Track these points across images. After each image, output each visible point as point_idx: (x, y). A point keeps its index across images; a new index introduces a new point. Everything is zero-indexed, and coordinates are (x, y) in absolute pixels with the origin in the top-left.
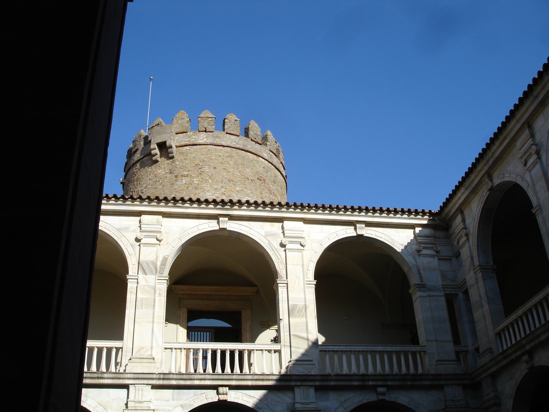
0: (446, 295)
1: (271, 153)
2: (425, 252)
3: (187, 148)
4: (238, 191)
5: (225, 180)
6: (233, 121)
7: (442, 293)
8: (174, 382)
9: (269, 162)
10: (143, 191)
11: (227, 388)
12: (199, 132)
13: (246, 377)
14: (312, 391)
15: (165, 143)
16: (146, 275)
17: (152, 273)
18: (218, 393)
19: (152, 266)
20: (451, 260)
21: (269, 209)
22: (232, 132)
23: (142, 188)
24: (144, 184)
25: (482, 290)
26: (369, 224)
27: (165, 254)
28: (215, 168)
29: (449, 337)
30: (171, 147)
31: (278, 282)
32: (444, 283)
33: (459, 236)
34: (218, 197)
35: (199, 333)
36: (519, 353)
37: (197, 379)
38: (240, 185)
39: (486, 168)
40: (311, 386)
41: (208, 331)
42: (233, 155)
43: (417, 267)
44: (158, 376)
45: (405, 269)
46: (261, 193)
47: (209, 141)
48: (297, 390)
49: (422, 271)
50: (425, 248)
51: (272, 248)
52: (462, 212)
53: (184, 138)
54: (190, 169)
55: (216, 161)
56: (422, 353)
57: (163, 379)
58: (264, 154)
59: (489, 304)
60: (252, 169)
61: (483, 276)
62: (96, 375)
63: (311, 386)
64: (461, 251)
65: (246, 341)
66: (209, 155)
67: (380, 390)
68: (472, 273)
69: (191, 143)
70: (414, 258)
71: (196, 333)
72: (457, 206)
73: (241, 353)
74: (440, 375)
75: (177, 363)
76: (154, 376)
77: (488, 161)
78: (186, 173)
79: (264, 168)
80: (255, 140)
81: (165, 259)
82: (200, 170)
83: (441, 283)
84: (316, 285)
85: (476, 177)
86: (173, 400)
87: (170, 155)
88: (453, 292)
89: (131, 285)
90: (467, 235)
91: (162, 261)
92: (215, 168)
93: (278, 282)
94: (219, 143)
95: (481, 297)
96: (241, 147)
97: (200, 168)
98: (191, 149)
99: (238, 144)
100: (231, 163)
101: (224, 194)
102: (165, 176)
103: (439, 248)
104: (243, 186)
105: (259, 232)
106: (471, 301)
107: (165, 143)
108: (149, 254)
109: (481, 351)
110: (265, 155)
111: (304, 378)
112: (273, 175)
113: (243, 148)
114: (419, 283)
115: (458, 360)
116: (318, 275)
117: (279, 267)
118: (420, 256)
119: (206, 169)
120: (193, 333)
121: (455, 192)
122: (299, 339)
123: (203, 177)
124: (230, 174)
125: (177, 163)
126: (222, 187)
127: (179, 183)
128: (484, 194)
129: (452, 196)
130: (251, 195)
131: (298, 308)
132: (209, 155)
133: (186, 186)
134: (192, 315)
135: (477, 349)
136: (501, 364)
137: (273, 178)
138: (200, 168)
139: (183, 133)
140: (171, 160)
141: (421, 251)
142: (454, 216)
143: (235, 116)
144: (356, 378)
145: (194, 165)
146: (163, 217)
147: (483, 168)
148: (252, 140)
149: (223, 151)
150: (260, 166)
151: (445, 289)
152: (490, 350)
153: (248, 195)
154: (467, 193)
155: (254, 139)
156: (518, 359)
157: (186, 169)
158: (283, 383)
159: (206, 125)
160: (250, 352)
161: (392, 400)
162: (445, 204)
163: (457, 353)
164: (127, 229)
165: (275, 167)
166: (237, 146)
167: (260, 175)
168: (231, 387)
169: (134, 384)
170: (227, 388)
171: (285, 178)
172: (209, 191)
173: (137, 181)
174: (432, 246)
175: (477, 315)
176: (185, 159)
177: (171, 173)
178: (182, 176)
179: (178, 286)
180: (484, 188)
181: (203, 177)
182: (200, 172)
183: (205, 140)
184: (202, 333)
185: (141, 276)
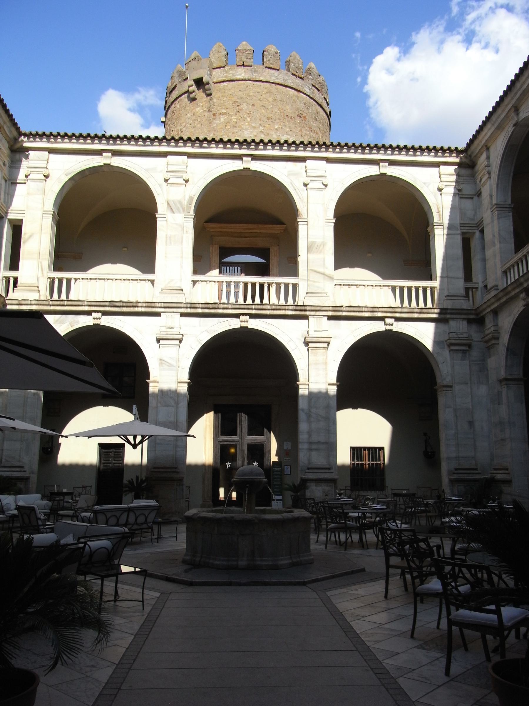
0: (463, 233)
1: (313, 88)
3: (225, 84)
4: (276, 129)
5: (263, 118)
6: (273, 54)
7: (459, 232)
8: (200, 311)
9: (311, 98)
10: (182, 130)
11: (394, 319)
12: (237, 66)
13: (264, 307)
14: (465, 323)
16: (174, 213)
17: (180, 212)
18: (386, 325)
19: (178, 205)
20: (472, 198)
21: (295, 149)
23: (181, 128)
24: (183, 123)
25: (496, 229)
26: (392, 163)
29: (461, 274)
30: (208, 83)
31: (298, 220)
32: (462, 222)
33: (482, 174)
34: (256, 136)
35: (228, 268)
36: (517, 290)
37: (220, 308)
38: (279, 122)
39: (513, 101)
40: (464, 319)
41: (239, 266)
42: (273, 91)
44: (185, 306)
46: (301, 131)
47: (247, 77)
51: (294, 188)
52: (488, 149)
54: (229, 106)
55: (254, 98)
56: (474, 290)
57: (190, 308)
59: (500, 242)
60: (292, 105)
61: (498, 215)
62: (226, 306)
63: (464, 319)
64: (482, 190)
65: (274, 275)
68: (489, 211)
69: (229, 79)
71: (231, 268)
72: (483, 142)
73: (262, 286)
76: (182, 305)
77: (516, 93)
78: (224, 111)
79: (305, 104)
81: (191, 198)
82: (237, 108)
83: (458, 222)
84: (335, 223)
85: (503, 111)
87: (208, 92)
89: (160, 224)
90: (489, 173)
92: (253, 105)
93: (298, 220)
94: (257, 78)
95: (494, 236)
96: (281, 82)
97: (238, 106)
98: (229, 85)
99: (277, 79)
100: (270, 99)
101: (263, 132)
102: (203, 115)
104: (282, 124)
105: (284, 173)
106: (485, 240)
109: (488, 288)
110: (307, 91)
112: (315, 111)
113: (283, 84)
115: (467, 296)
116: (337, 215)
117: (300, 205)
119: (244, 106)
120: (233, 268)
121: (481, 128)
122: (315, 273)
124: (268, 111)
125: (215, 100)
126: (260, 125)
127: (217, 121)
128: (510, 129)
129: (478, 132)
130: (290, 133)
131: (316, 245)
133: (224, 124)
134: (225, 252)
135: (486, 286)
136: (502, 301)
137: (314, 115)
138: (238, 106)
139: (220, 68)
140: (209, 98)
142: (480, 153)
143: (275, 47)
144: (367, 309)
145: (231, 102)
146: (188, 157)
147: (510, 102)
148: (293, 74)
149: (262, 87)
150: (301, 102)
151: (462, 228)
152: (495, 287)
153: (287, 133)
154: (493, 129)
155: (295, 73)
156: (517, 296)
157: (224, 107)
158: (443, 316)
159: (244, 59)
160: (269, 285)
162: (472, 141)
163: (467, 289)
165: (317, 103)
166: (277, 81)
167: (301, 112)
168: (252, 316)
170: (394, 319)
171: (329, 116)
172: (246, 129)
173: (176, 119)
175: (489, 253)
176: (222, 96)
177: (209, 111)
178: (220, 114)
179: (209, 224)
180: (510, 123)
181: (240, 114)
182: (238, 110)
184: (236, 268)
185: (169, 215)
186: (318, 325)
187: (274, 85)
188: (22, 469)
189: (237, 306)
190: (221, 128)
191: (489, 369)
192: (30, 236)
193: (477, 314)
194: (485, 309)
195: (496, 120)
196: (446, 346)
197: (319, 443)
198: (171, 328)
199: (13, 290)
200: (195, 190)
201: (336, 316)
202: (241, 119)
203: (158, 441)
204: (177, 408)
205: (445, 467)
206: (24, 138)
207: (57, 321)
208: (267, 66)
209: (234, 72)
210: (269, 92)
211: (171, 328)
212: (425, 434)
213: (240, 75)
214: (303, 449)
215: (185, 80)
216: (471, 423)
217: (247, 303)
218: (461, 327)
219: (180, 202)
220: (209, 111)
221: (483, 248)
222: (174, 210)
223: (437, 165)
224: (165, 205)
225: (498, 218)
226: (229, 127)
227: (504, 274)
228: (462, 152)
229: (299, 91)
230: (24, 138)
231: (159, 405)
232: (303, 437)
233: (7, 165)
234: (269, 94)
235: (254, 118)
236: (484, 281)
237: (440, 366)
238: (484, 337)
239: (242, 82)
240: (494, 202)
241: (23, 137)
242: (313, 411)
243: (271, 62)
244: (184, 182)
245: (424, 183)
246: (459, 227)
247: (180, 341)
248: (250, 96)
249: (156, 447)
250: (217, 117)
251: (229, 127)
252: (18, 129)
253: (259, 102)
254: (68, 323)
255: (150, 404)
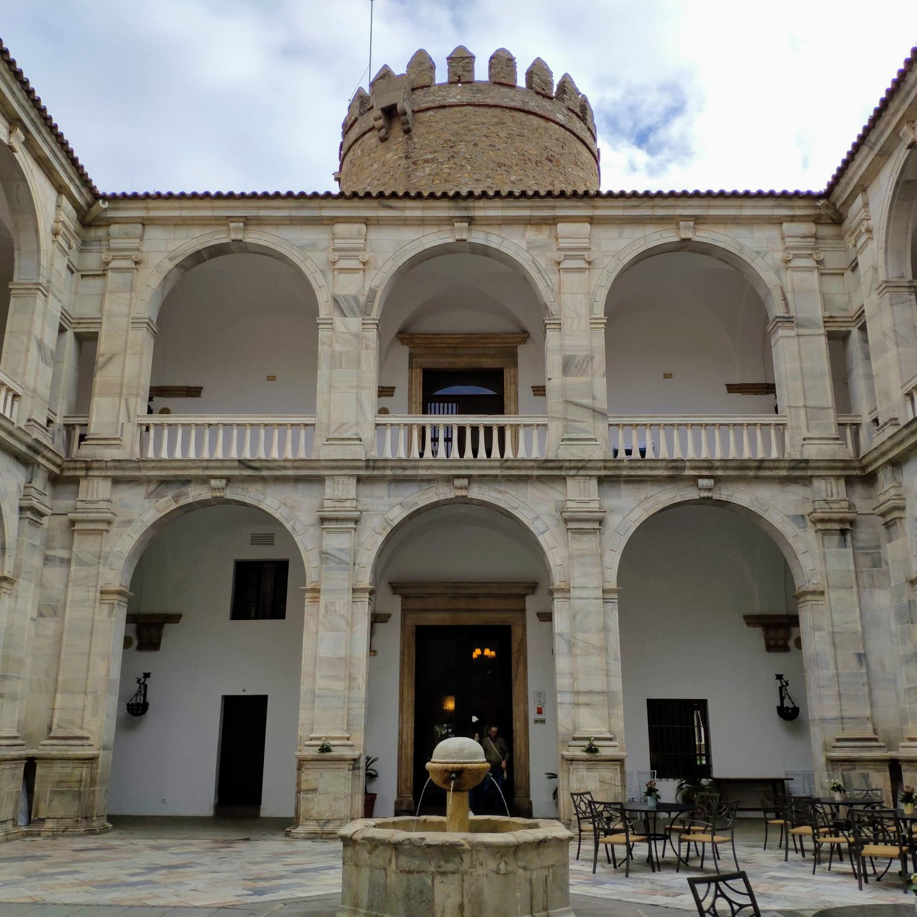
2: (797, 263)
3: (430, 113)
7: (822, 331)
15: (394, 106)
17: (356, 316)
19: (353, 303)
20: (843, 274)
22: (504, 81)
27: (373, 284)
28: (476, 145)
30: (405, 113)
32: (827, 314)
40: (838, 477)
43: (782, 289)
45: (762, 294)
47: (465, 100)
48: (569, 482)
49: (789, 296)
50: (796, 256)
51: (538, 269)
53: (424, 96)
55: (477, 133)
58: (558, 115)
60: (537, 143)
61: (891, 299)
66: (465, 124)
67: (702, 482)
69: (437, 104)
70: (778, 273)
74: (807, 461)
75: (395, 448)
78: (430, 156)
80: (543, 92)
81: (373, 292)
86: (389, 496)
88: (843, 329)
91: (368, 296)
92: (476, 145)
94: (482, 101)
97: (452, 147)
99: (513, 100)
100: (503, 134)
103: (822, 256)
104: (521, 172)
105: (514, 244)
107: (394, 106)
108: (350, 285)
109: (881, 422)
110: (560, 117)
111: (580, 464)
114: (782, 315)
118: (787, 268)
121: (852, 155)
123: (456, 160)
124: (499, 153)
125: (415, 140)
126: (488, 177)
127: (420, 174)
129: (846, 163)
131: (576, 361)
132: (465, 124)
135: (876, 421)
138: (452, 147)
141: (789, 261)
145: (442, 142)
148: (538, 93)
152: (894, 421)
155: (539, 90)
161: (724, 498)
162: (837, 179)
164: (313, 246)
166: (512, 104)
167: (552, 153)
169: (332, 476)
174: (810, 252)
178: (426, 161)
181: (456, 160)
183: (459, 97)
185: (338, 320)
186: (581, 494)
187: (508, 111)
188: (85, 742)
189: (449, 464)
190: (426, 184)
191: (889, 562)
192: (109, 360)
193: (863, 468)
194: (876, 460)
195: (877, 140)
196: (809, 523)
197: (590, 692)
198: (341, 501)
199: (80, 445)
200: (379, 277)
201: (611, 476)
202: (458, 168)
203: (317, 692)
204: (352, 633)
205: (818, 735)
206: (104, 203)
207: (152, 493)
208: (497, 80)
209: (445, 93)
210: (501, 123)
211: (341, 501)
212: (779, 677)
213: (455, 97)
214: (564, 704)
215: (369, 110)
216: (862, 658)
217: (451, 458)
218: (835, 491)
219: (355, 298)
220: (406, 157)
221: (867, 357)
222: (345, 311)
223: (779, 221)
224: (331, 303)
225: (891, 305)
226: (438, 182)
227: (908, 398)
228: (820, 196)
229: (548, 119)
230: (104, 203)
231: (320, 629)
232: (562, 682)
233: (75, 247)
234: (500, 126)
235: (476, 165)
236: (872, 412)
237: (800, 557)
238: (877, 507)
239: (458, 109)
240: (882, 277)
241: (101, 201)
242: (579, 636)
243: (502, 75)
244: (362, 267)
245: (758, 252)
246: (822, 324)
247: (356, 521)
248: (470, 130)
249: (314, 702)
250: (419, 166)
251: (438, 182)
252: (92, 189)
253: (485, 139)
254: (170, 497)
255: (305, 629)
